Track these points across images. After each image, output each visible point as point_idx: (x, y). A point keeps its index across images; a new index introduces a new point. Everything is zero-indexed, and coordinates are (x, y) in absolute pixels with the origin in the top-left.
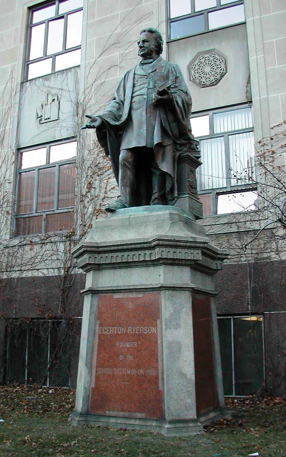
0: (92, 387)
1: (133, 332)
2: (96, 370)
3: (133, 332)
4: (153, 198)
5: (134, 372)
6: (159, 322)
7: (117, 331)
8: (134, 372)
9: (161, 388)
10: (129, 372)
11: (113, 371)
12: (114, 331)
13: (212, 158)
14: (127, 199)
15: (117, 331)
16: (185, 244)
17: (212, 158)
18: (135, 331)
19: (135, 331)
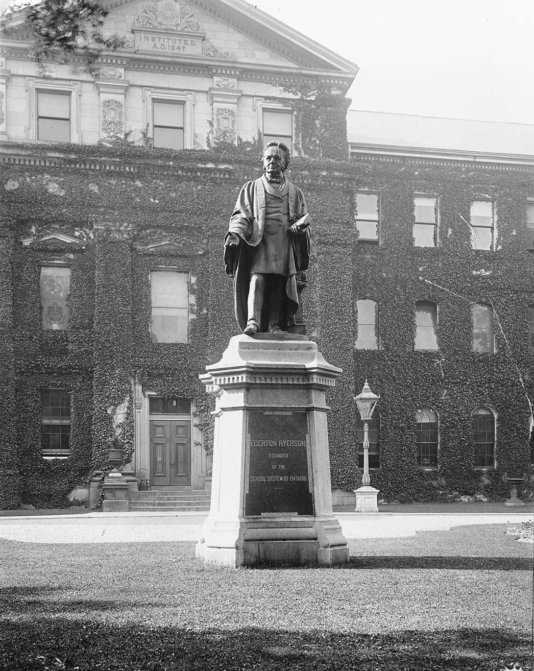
0: (247, 494)
1: (283, 444)
2: (250, 478)
3: (283, 444)
4: (249, 206)
5: (286, 478)
6: (307, 436)
7: (268, 444)
8: (286, 478)
9: (311, 491)
10: (281, 479)
11: (266, 479)
12: (266, 443)
13: (227, 548)
14: (68, 97)
15: (268, 444)
16: (334, 56)
17: (227, 548)
18: (286, 444)
19: (286, 444)
